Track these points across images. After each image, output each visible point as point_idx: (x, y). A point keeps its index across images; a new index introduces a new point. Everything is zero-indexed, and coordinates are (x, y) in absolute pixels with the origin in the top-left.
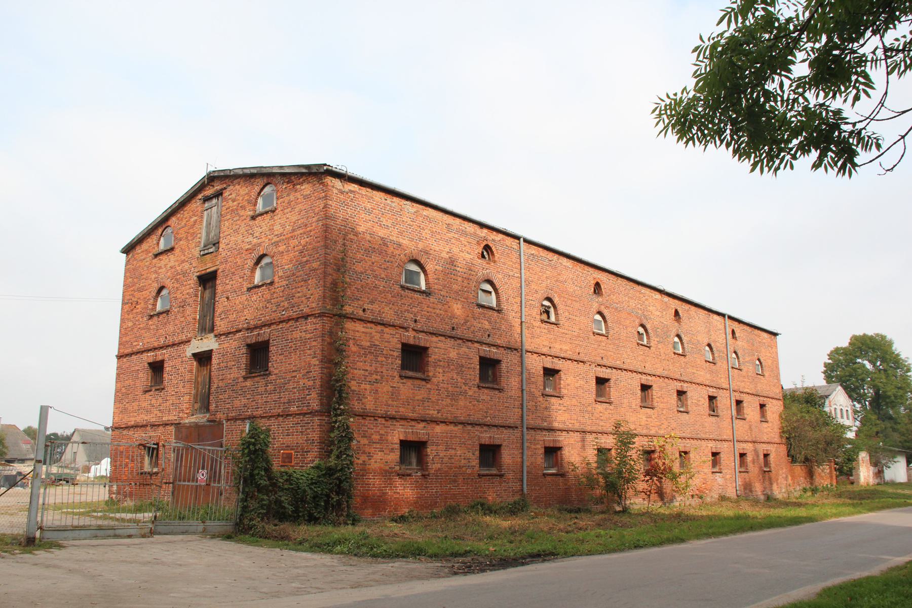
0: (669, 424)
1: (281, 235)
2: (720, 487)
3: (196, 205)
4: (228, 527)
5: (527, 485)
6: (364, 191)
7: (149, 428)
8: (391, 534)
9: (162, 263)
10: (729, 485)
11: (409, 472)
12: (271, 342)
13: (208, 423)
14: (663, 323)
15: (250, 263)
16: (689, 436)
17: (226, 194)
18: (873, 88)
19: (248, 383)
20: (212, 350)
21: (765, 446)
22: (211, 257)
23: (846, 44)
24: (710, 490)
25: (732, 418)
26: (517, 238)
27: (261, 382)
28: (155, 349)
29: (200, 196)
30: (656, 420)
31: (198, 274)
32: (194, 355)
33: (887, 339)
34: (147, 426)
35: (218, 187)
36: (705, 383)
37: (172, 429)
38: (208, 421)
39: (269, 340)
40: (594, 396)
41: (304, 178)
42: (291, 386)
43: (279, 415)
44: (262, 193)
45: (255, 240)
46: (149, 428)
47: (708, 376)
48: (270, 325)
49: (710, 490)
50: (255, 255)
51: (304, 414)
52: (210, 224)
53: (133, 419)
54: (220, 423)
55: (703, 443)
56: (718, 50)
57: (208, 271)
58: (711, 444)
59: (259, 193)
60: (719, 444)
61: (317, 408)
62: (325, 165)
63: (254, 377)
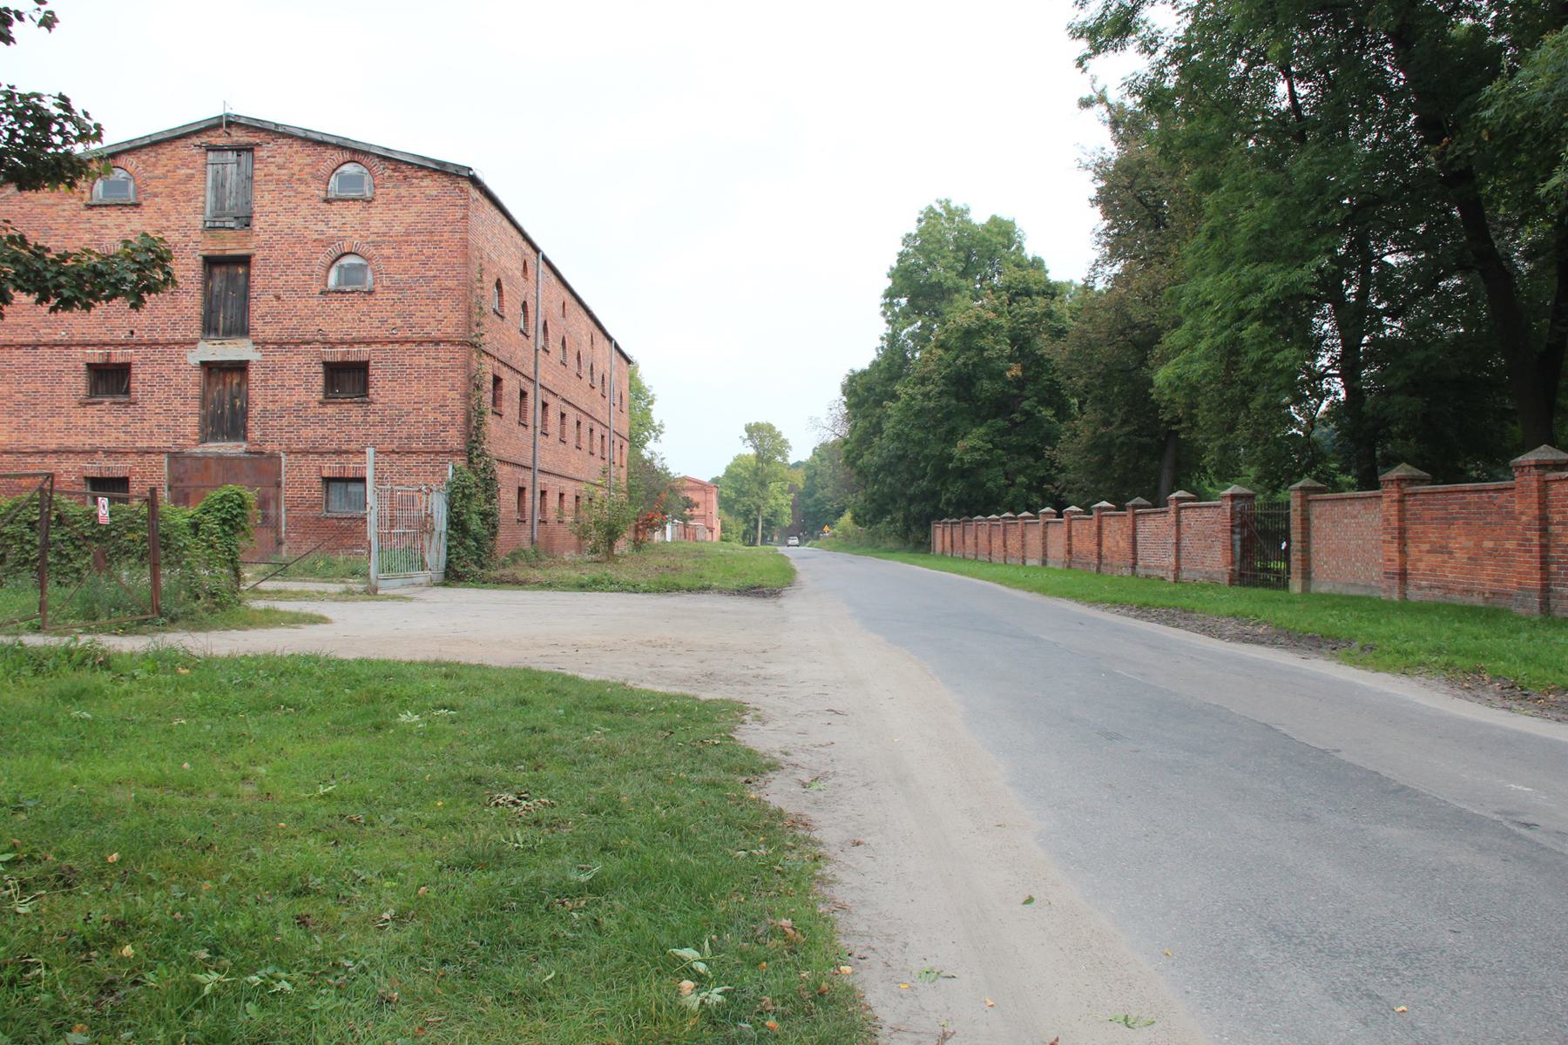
1: (384, 234)
3: (183, 150)
4: (440, 577)
5: (1287, 519)
6: (486, 202)
7: (101, 455)
8: (673, 566)
9: (109, 221)
12: (372, 363)
13: (247, 455)
15: (324, 259)
17: (260, 153)
19: (330, 410)
20: (248, 361)
22: (234, 235)
23: (1284, 545)
26: (537, 250)
27: (356, 413)
28: (105, 344)
29: (204, 139)
31: (205, 253)
32: (204, 364)
33: (13, 184)
34: (96, 452)
35: (240, 137)
37: (165, 459)
38: (246, 452)
41: (425, 173)
42: (413, 419)
43: (393, 452)
44: (338, 171)
45: (332, 232)
46: (101, 455)
48: (368, 344)
50: (334, 250)
51: (437, 453)
52: (223, 186)
53: (55, 441)
54: (274, 457)
57: (228, 253)
59: (335, 170)
61: (456, 446)
62: (470, 169)
63: (341, 403)
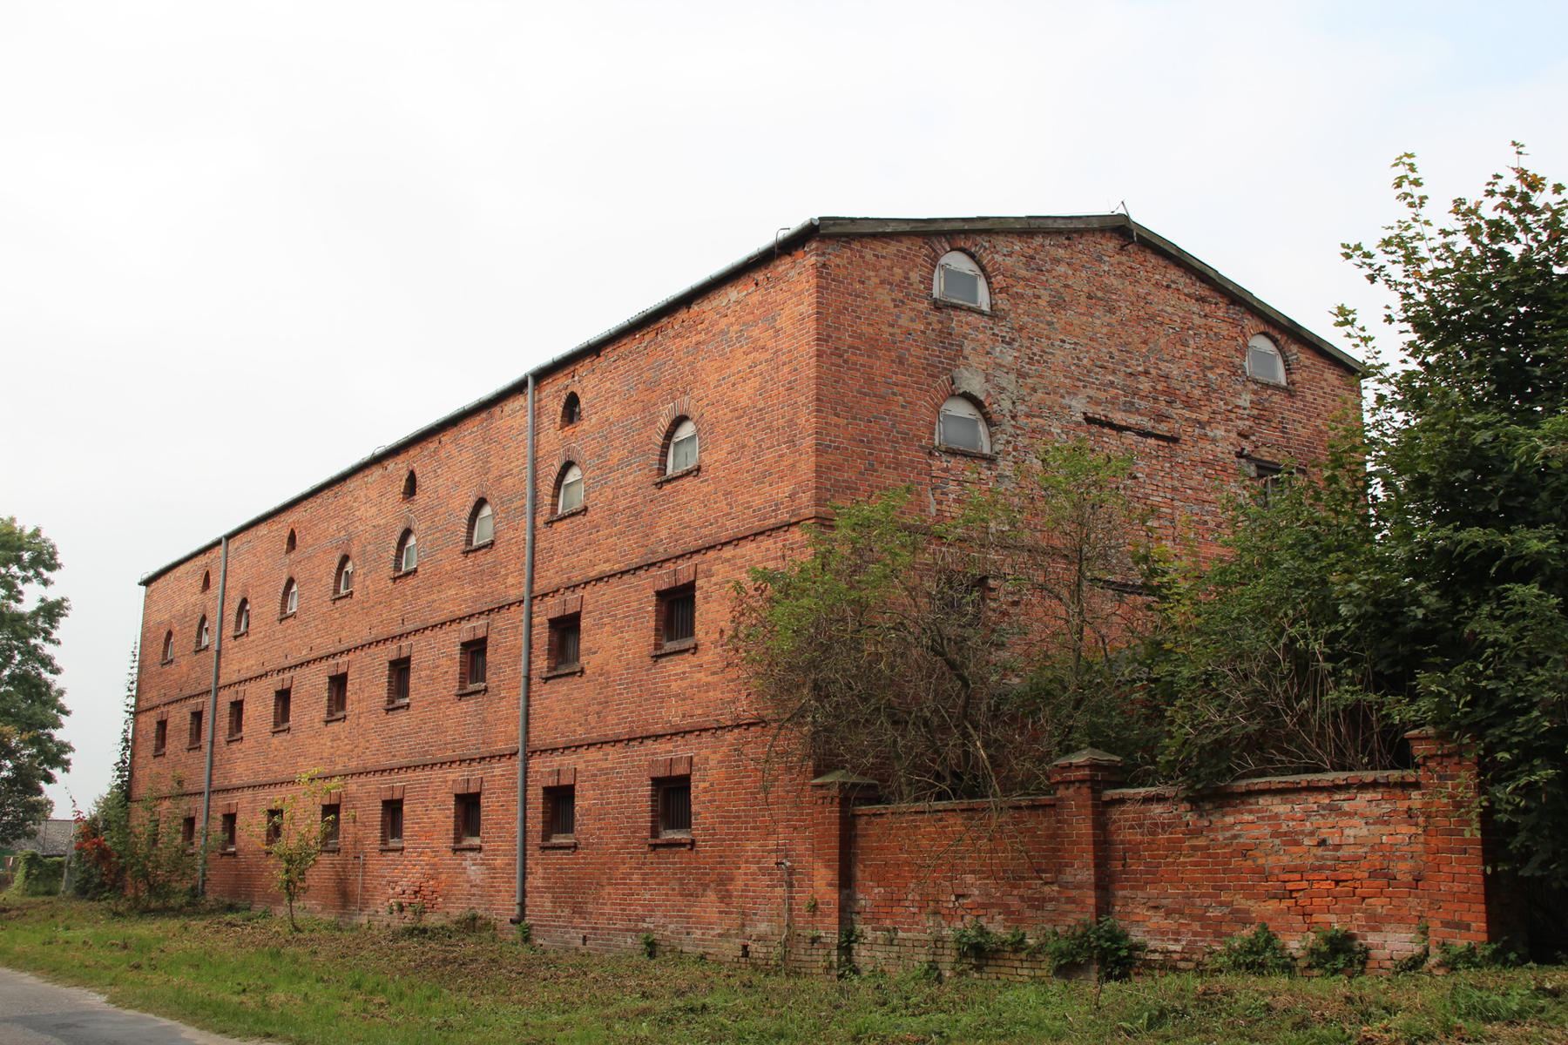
0: (368, 745)
2: (474, 890)
10: (503, 887)
11: (218, 824)
14: (379, 526)
16: (404, 762)
18: (1342, 254)
21: (669, 746)
24: (446, 897)
25: (528, 678)
30: (346, 741)
36: (459, 614)
39: (694, 581)
40: (384, 693)
47: (469, 591)
49: (446, 897)
55: (437, 774)
56: (1499, 755)
58: (456, 774)
60: (477, 771)
